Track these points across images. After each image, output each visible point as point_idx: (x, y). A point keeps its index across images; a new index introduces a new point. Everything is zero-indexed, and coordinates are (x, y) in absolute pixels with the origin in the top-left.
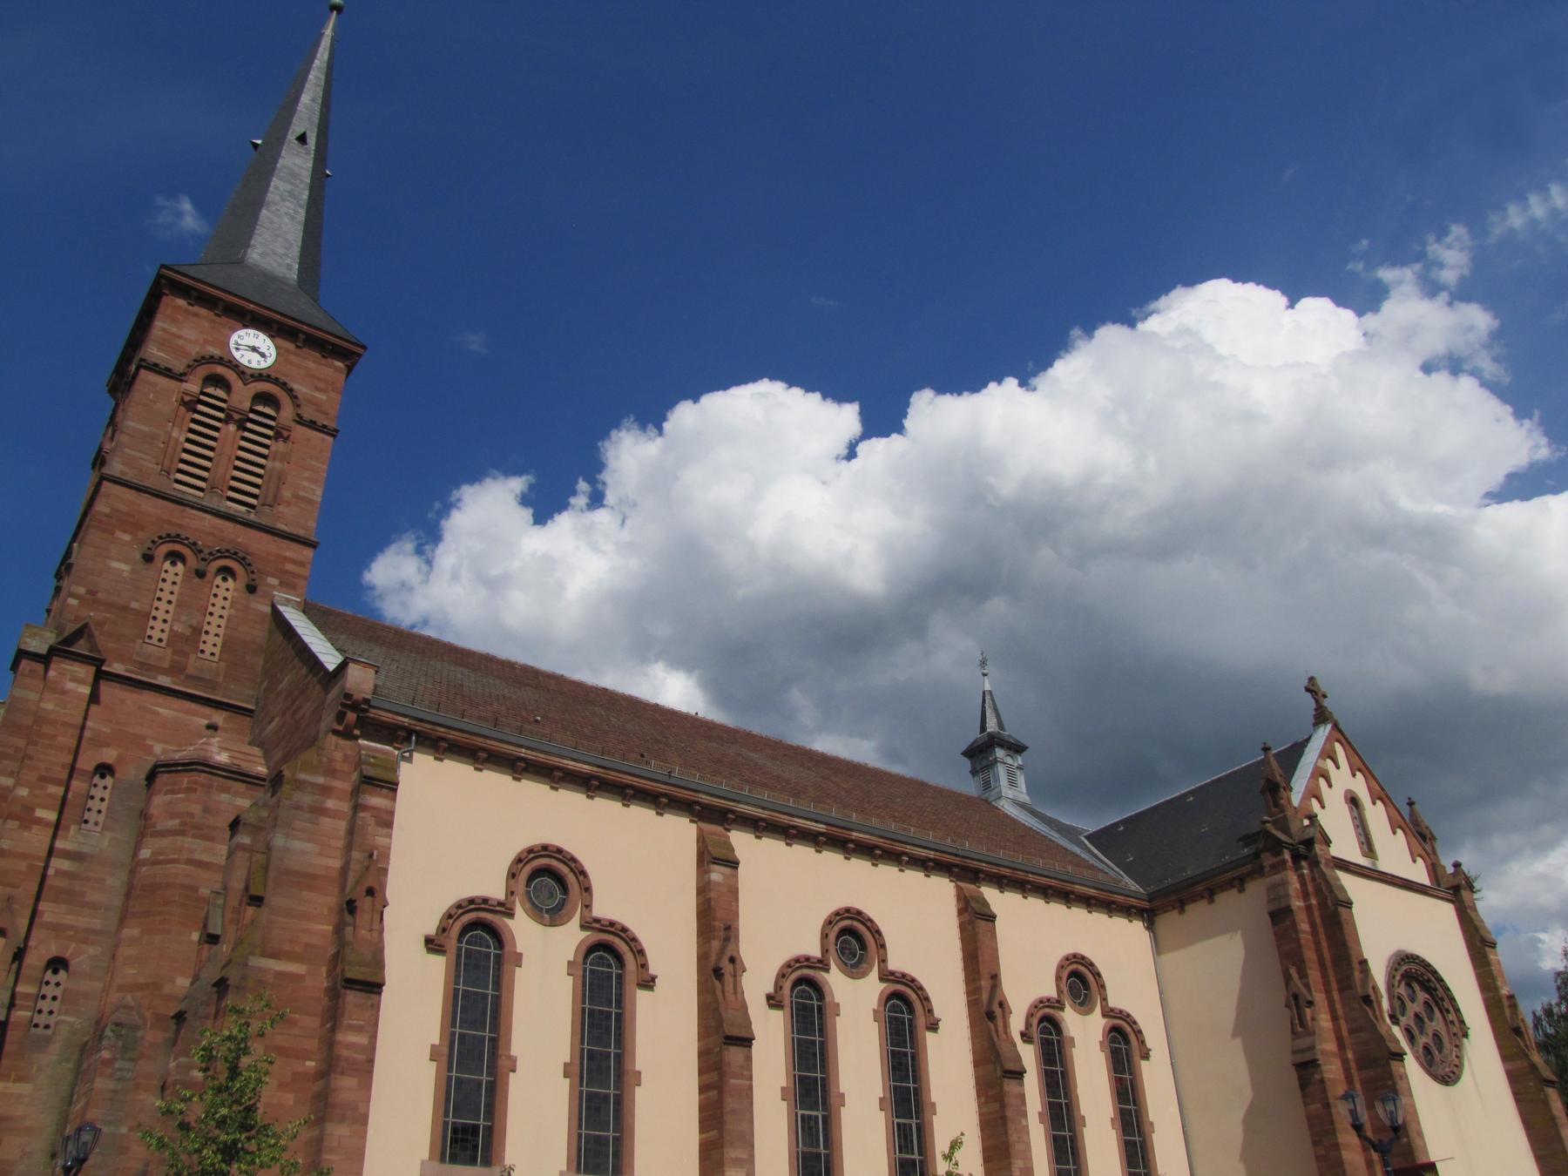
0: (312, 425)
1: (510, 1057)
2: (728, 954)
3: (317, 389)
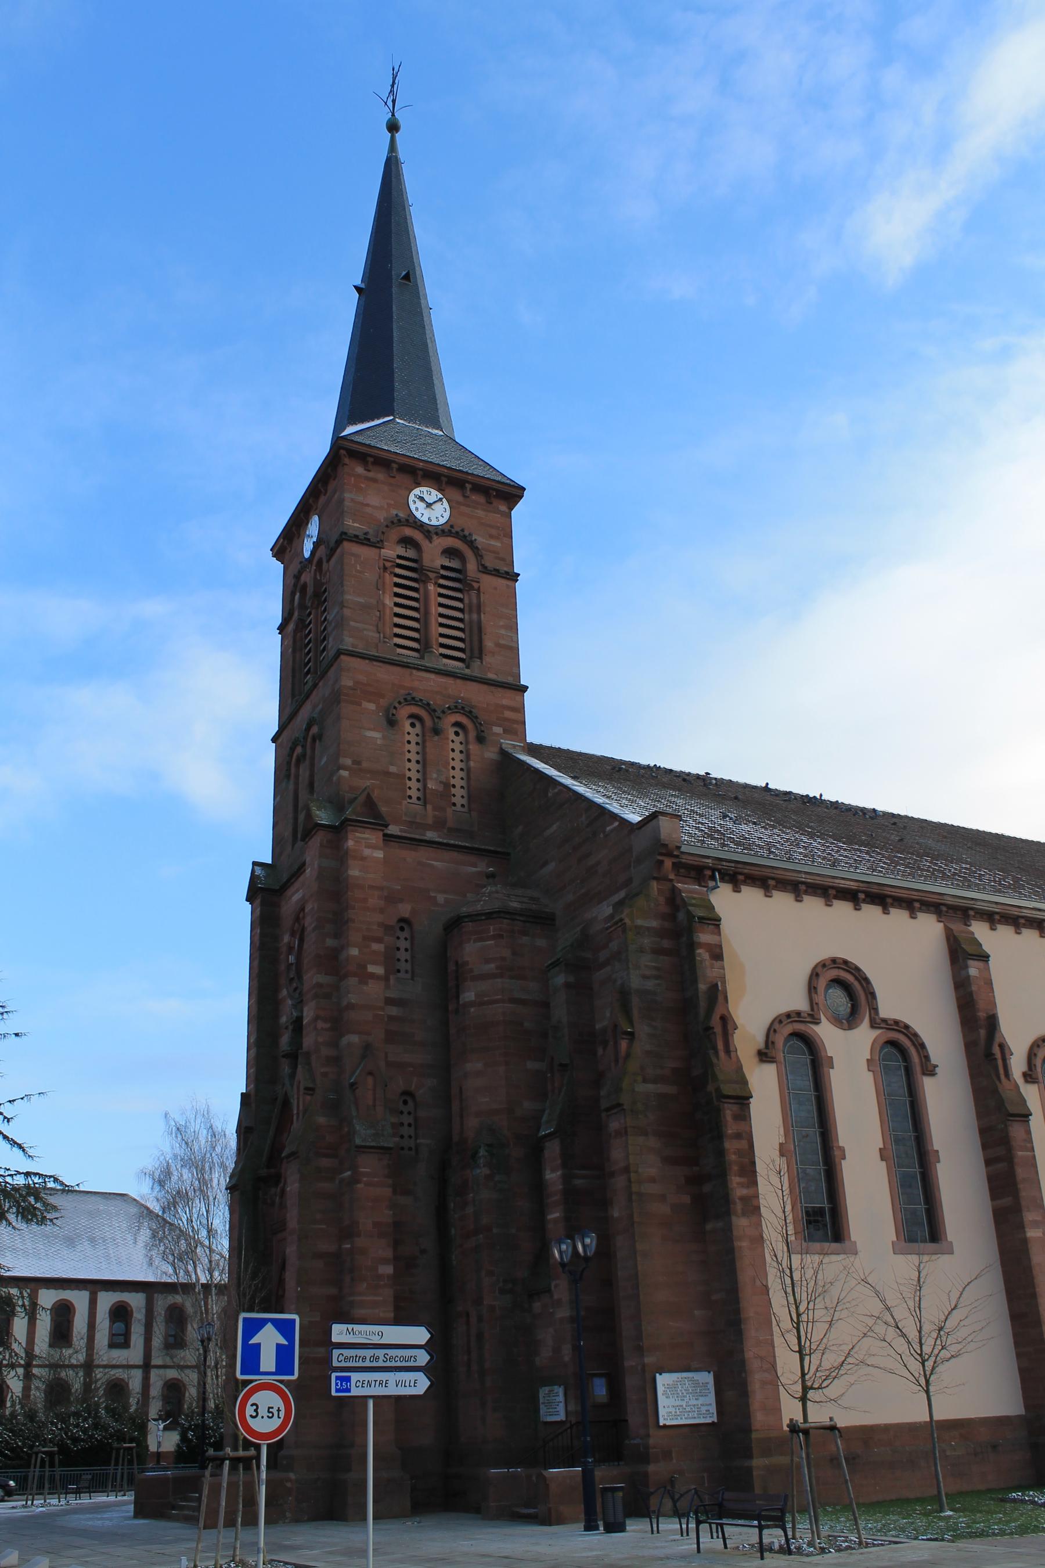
0: (496, 573)
1: (840, 1147)
2: (997, 1040)
3: (491, 537)
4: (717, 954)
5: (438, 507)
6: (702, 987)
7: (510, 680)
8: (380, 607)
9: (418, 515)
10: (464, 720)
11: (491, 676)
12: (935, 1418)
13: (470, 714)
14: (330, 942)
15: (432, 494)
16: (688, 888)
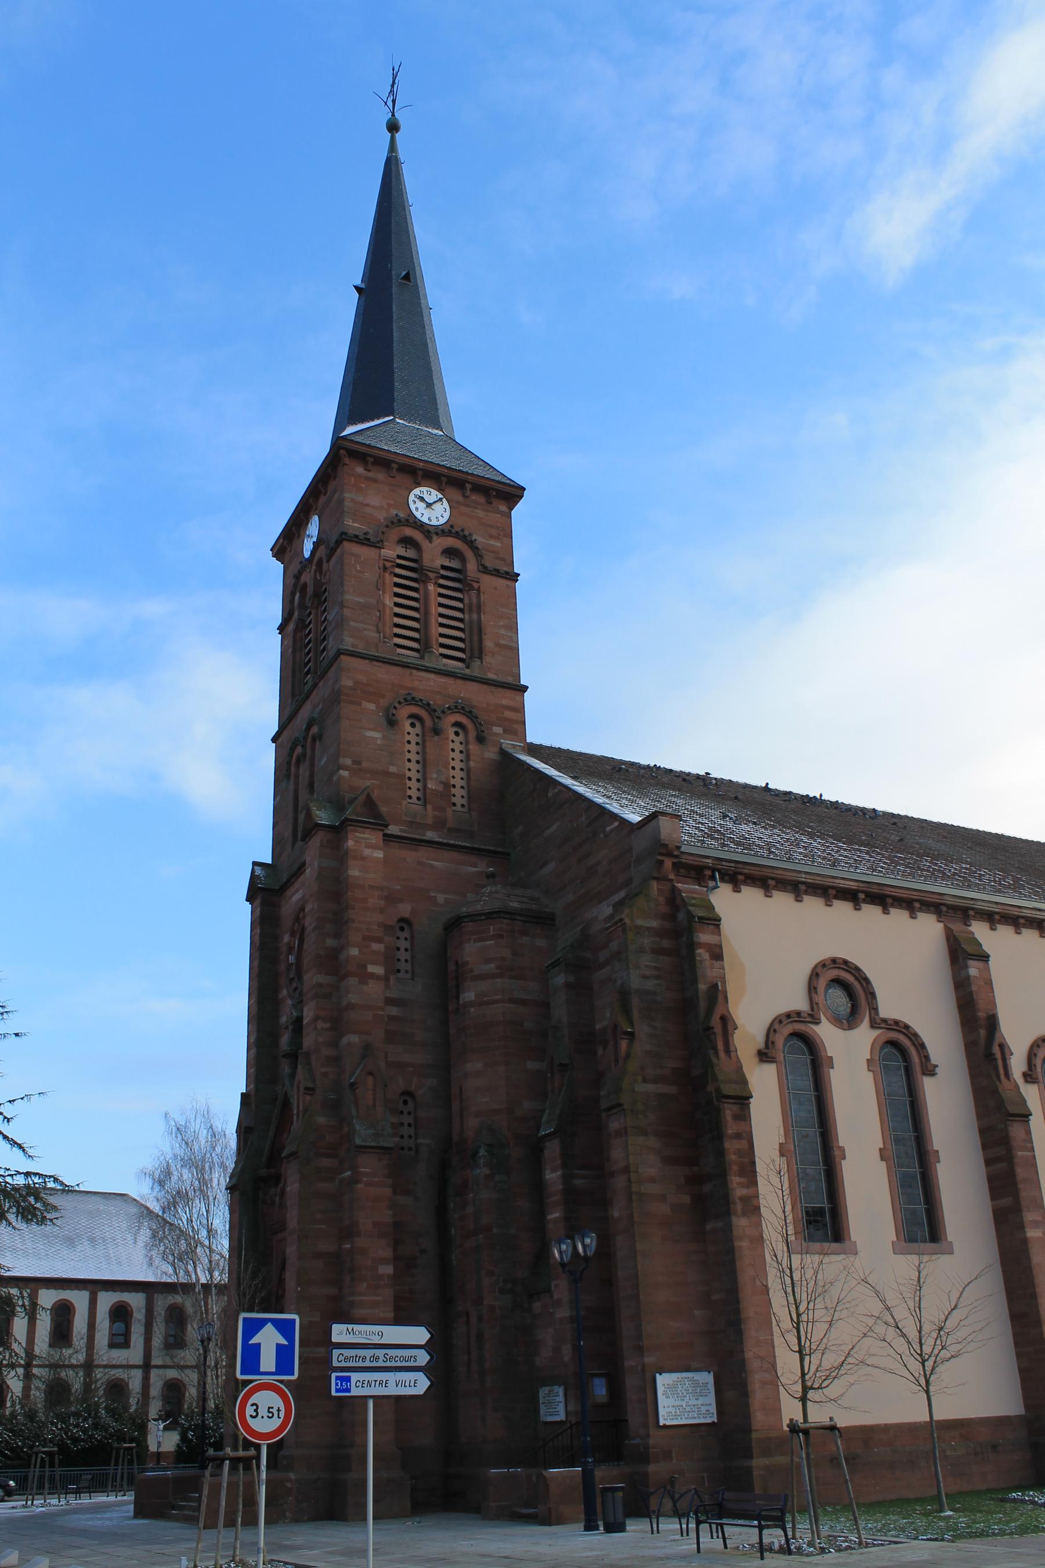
0: (497, 573)
1: (840, 1147)
3: (491, 537)
4: (717, 955)
5: (438, 507)
6: (702, 987)
7: (510, 680)
8: (380, 607)
9: (418, 515)
10: (464, 720)
11: (491, 676)
12: (935, 1418)
13: (470, 714)
14: (330, 942)
15: (432, 494)
16: (688, 888)
